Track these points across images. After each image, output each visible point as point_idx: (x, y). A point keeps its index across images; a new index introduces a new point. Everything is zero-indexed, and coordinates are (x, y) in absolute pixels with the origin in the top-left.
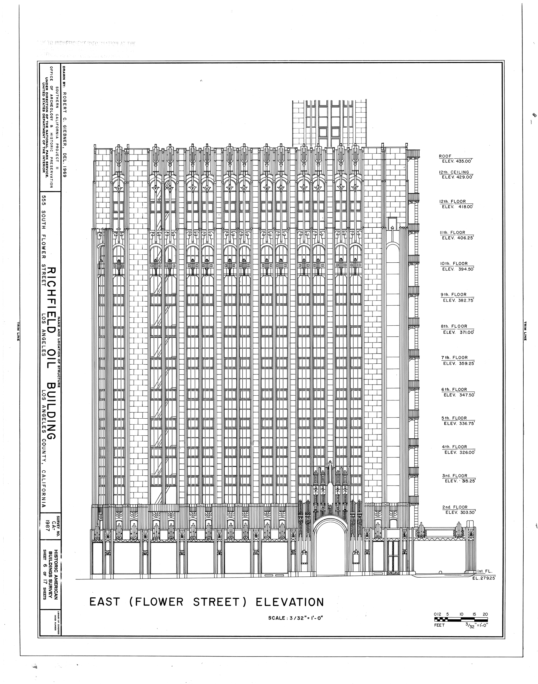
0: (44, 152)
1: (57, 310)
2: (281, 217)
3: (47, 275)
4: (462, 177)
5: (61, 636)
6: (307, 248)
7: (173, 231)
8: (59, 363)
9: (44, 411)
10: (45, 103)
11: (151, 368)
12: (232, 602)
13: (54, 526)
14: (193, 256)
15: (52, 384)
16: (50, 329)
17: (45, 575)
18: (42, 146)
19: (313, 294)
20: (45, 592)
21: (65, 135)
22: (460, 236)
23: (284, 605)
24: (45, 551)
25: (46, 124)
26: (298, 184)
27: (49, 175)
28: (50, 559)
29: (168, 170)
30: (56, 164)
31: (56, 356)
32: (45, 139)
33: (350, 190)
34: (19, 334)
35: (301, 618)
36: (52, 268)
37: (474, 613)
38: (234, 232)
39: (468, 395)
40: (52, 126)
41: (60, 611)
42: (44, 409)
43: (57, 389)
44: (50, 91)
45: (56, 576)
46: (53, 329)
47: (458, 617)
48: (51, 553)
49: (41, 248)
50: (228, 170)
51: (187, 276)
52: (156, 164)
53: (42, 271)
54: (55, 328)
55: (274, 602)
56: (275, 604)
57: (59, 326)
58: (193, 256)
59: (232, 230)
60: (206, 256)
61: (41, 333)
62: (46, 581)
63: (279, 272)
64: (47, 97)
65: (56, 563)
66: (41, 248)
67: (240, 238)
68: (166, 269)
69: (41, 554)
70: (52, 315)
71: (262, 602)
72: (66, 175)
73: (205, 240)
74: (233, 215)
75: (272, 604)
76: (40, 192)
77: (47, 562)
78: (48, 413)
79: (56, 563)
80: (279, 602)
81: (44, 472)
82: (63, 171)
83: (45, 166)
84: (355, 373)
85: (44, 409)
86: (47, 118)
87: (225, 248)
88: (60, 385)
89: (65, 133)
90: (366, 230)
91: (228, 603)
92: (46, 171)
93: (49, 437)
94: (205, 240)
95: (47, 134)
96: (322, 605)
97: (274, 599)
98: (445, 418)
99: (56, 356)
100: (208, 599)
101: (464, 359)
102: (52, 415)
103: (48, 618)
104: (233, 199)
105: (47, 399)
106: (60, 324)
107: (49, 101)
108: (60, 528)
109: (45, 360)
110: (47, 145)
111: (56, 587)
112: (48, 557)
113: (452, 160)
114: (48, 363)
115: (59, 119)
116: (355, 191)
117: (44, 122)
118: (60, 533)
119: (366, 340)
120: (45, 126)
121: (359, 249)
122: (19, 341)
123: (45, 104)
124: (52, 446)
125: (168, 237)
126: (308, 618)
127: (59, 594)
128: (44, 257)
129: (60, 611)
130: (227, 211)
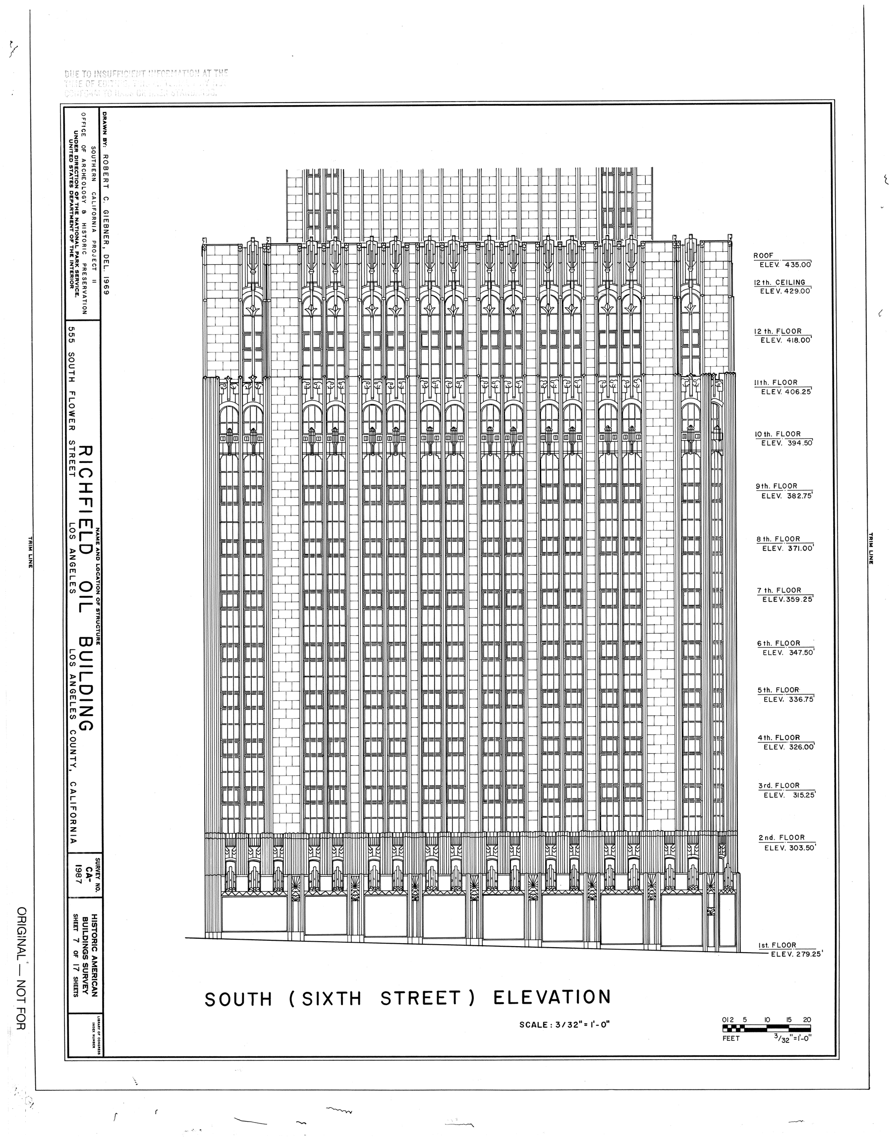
0: (72, 255)
1: (95, 516)
2: (632, 355)
3: (78, 458)
4: (794, 292)
5: (103, 1057)
6: (577, 408)
7: (495, 380)
8: (98, 604)
9: (73, 684)
10: (73, 173)
11: (305, 608)
12: (448, 998)
13: (89, 876)
14: (430, 421)
15: (86, 638)
16: (83, 549)
17: (76, 955)
18: (69, 244)
19: (623, 484)
20: (76, 985)
21: (107, 226)
22: (790, 389)
23: (542, 1002)
24: (76, 916)
25: (75, 209)
26: (598, 301)
27: (81, 294)
28: (85, 930)
29: (628, 278)
30: (93, 275)
31: (93, 593)
32: (73, 233)
33: (563, 314)
34: (31, 557)
35: (573, 1025)
36: (86, 447)
37: (789, 1018)
38: (319, 384)
39: (803, 652)
40: (84, 212)
41: (101, 1015)
42: (73, 680)
43: (96, 648)
44: (80, 154)
45: (95, 958)
46: (89, 549)
47: (761, 1023)
48: (85, 919)
49: (68, 415)
50: (427, 279)
51: (364, 455)
52: (631, 269)
53: (69, 451)
54: (92, 546)
55: (524, 997)
56: (526, 1000)
57: (97, 543)
58: (430, 421)
59: (635, 376)
60: (451, 421)
61: (69, 554)
62: (77, 967)
63: (510, 450)
64: (77, 164)
65: (94, 935)
66: (68, 414)
67: (447, 392)
68: (447, 444)
69: (69, 921)
70: (86, 525)
71: (504, 998)
72: (108, 292)
73: (450, 396)
74: (495, 353)
75: (520, 1001)
76: (66, 320)
77: (79, 934)
78: (81, 686)
79: (94, 935)
80: (533, 997)
81: (73, 784)
82: (103, 284)
83: (74, 278)
84: (632, 616)
85: (73, 680)
86: (77, 198)
87: (625, 406)
88: (100, 641)
89: (106, 223)
90: (649, 379)
91: (441, 1000)
92: (75, 285)
93: (83, 727)
94: (450, 396)
95: (77, 224)
96: (608, 1001)
97: (524, 992)
98: (763, 691)
99: (93, 593)
100: (407, 994)
101: (796, 593)
102: (88, 690)
103: (82, 1028)
104: (435, 327)
105: (78, 665)
106: (100, 540)
107: (80, 170)
108: (101, 878)
109: (74, 600)
110: (77, 243)
111: (95, 975)
112: (80, 927)
113: (777, 262)
114: (81, 604)
115: (97, 200)
116: (691, 314)
117: (72, 205)
118: (100, 887)
119: (650, 560)
120: (74, 211)
121: (637, 409)
122: (31, 569)
123: (74, 174)
124: (87, 742)
125: (451, 389)
126: (586, 1024)
127: (99, 987)
128: (73, 428)
129: (101, 1015)
130: (308, 349)
